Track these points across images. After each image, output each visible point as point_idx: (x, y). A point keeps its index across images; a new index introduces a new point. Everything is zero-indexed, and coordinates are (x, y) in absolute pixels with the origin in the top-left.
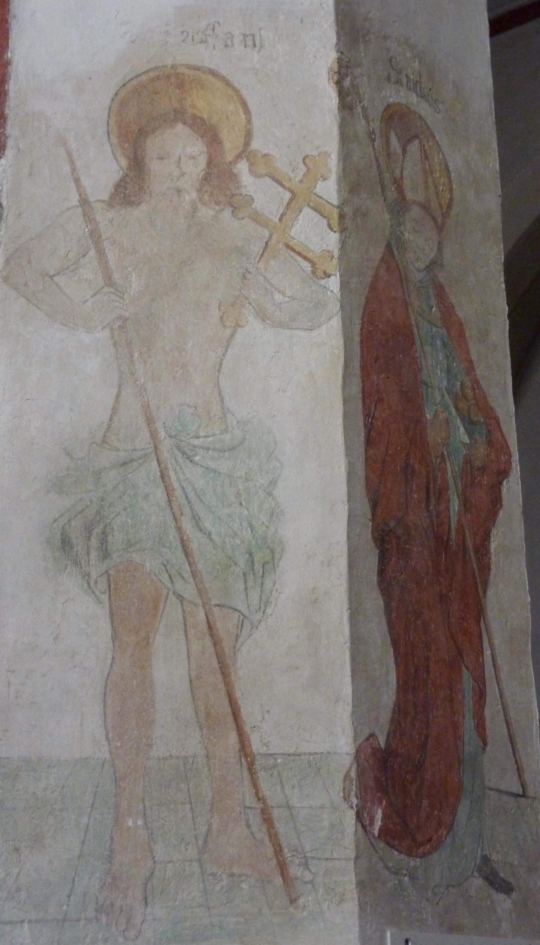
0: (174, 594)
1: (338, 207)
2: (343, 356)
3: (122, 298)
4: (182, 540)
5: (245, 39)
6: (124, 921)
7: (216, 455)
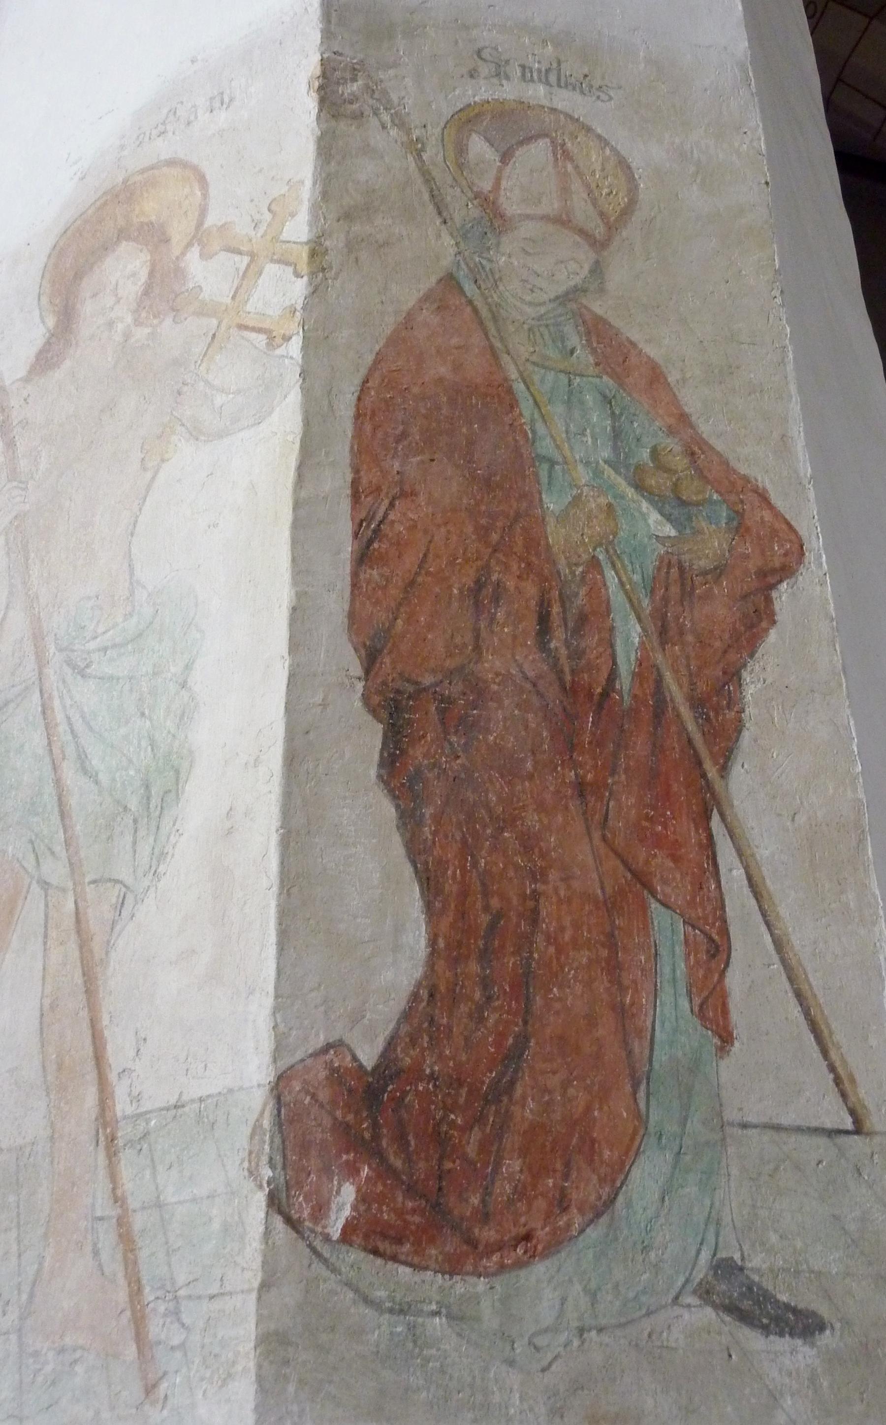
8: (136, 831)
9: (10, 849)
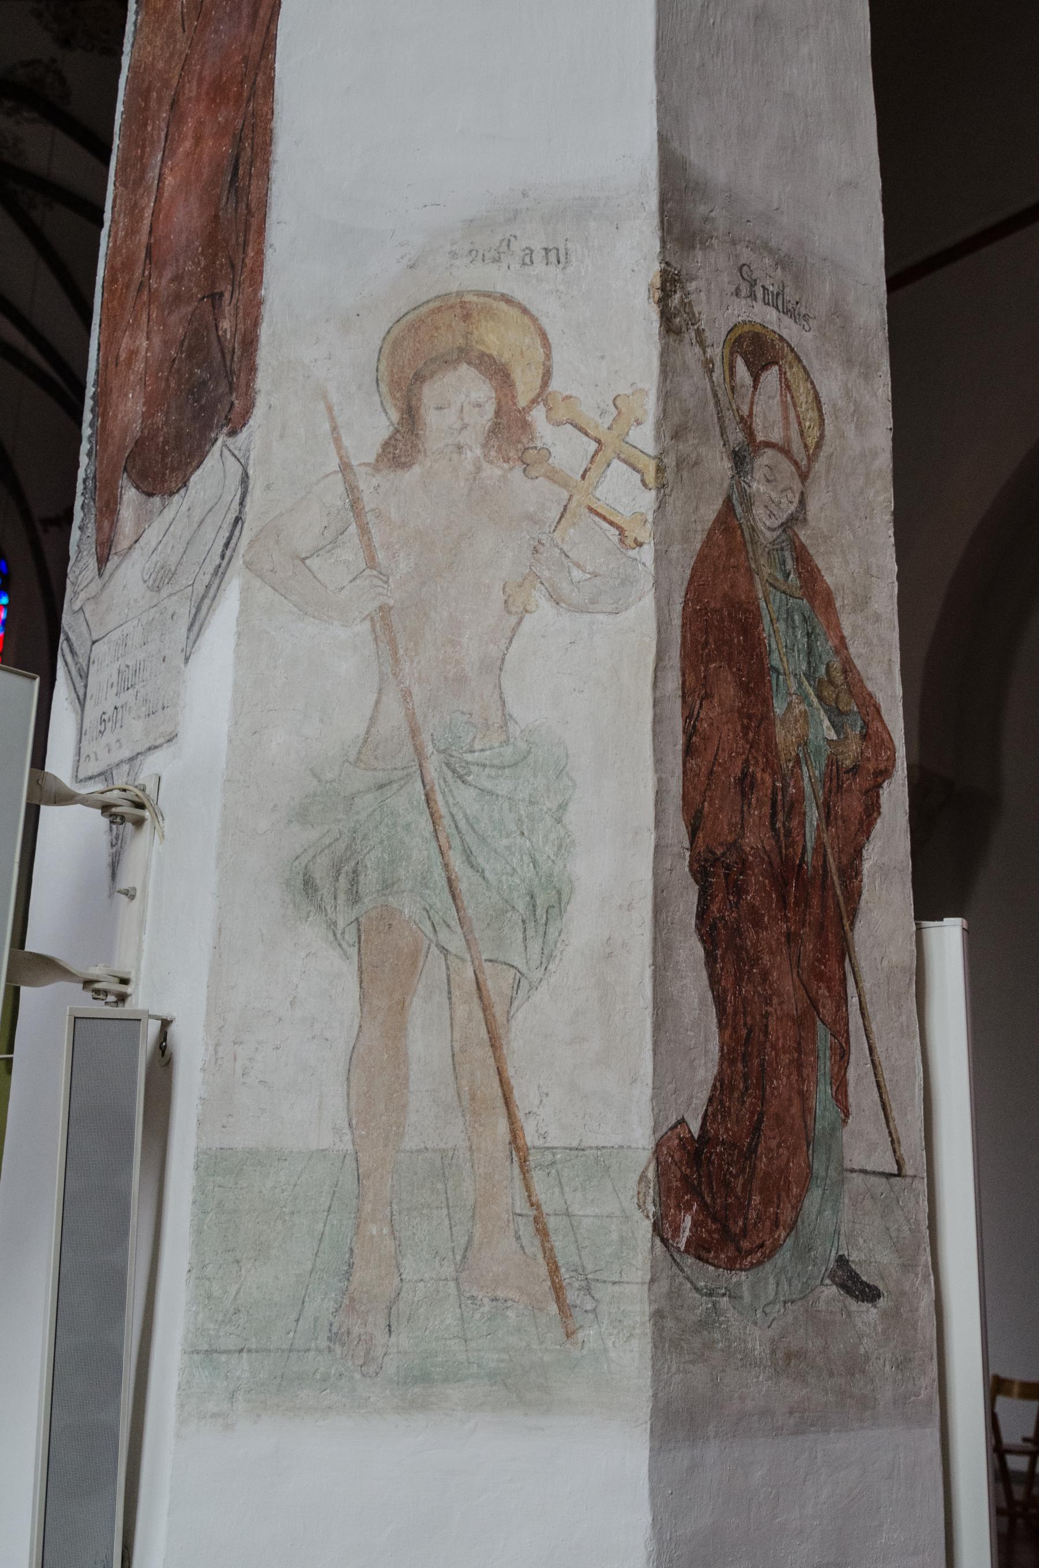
0: (437, 946)
1: (655, 458)
2: (655, 646)
3: (386, 582)
4: (449, 880)
5: (547, 254)
6: (362, 1354)
7: (493, 772)
8: (525, 931)
9: (406, 911)
